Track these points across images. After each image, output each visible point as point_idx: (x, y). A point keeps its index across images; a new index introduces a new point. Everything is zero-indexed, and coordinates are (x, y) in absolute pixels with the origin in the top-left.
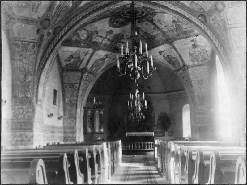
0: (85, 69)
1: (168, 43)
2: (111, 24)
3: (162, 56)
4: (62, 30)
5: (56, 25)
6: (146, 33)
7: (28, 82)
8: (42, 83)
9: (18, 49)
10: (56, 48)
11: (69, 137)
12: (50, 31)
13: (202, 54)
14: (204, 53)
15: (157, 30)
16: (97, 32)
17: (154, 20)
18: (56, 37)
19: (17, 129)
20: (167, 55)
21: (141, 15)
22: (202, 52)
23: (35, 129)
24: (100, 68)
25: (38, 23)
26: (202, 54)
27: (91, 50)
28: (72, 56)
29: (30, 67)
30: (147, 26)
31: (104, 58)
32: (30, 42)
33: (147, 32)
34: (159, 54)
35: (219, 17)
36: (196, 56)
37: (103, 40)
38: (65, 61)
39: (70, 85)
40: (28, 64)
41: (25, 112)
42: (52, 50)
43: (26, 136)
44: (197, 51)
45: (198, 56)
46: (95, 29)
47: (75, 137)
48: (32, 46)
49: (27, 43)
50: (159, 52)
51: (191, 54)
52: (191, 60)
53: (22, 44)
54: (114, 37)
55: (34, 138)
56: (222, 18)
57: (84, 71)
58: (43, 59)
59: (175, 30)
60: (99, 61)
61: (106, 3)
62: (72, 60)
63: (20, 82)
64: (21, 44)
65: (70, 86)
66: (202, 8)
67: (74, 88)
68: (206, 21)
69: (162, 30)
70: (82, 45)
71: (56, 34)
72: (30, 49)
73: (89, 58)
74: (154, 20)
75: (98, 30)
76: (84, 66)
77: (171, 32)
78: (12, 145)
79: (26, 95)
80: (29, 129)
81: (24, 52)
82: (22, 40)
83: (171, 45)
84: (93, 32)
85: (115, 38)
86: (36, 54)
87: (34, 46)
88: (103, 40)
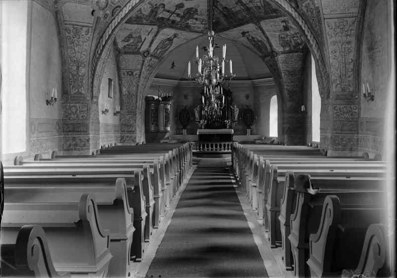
0: (148, 51)
1: (253, 23)
3: (246, 37)
5: (115, 4)
6: (225, 8)
9: (69, 35)
10: (114, 33)
12: (108, 12)
13: (295, 38)
14: (297, 37)
18: (114, 19)
20: (252, 37)
22: (295, 35)
23: (90, 132)
24: (167, 50)
26: (295, 38)
27: (155, 28)
28: (130, 36)
32: (83, 26)
35: (313, 4)
37: (170, 16)
38: (123, 41)
39: (128, 72)
40: (81, 53)
41: (78, 111)
44: (289, 34)
45: (290, 40)
48: (86, 31)
50: (242, 33)
51: (281, 37)
52: (282, 46)
53: (74, 28)
54: (185, 12)
56: (317, 6)
57: (146, 55)
58: (99, 46)
62: (132, 40)
63: (72, 75)
65: (128, 72)
67: (134, 76)
68: (298, 7)
70: (145, 21)
71: (115, 16)
73: (153, 38)
76: (147, 47)
78: (65, 150)
79: (80, 90)
82: (74, 23)
83: (256, 25)
84: (158, 5)
85: (187, 13)
87: (87, 32)
88: (170, 16)
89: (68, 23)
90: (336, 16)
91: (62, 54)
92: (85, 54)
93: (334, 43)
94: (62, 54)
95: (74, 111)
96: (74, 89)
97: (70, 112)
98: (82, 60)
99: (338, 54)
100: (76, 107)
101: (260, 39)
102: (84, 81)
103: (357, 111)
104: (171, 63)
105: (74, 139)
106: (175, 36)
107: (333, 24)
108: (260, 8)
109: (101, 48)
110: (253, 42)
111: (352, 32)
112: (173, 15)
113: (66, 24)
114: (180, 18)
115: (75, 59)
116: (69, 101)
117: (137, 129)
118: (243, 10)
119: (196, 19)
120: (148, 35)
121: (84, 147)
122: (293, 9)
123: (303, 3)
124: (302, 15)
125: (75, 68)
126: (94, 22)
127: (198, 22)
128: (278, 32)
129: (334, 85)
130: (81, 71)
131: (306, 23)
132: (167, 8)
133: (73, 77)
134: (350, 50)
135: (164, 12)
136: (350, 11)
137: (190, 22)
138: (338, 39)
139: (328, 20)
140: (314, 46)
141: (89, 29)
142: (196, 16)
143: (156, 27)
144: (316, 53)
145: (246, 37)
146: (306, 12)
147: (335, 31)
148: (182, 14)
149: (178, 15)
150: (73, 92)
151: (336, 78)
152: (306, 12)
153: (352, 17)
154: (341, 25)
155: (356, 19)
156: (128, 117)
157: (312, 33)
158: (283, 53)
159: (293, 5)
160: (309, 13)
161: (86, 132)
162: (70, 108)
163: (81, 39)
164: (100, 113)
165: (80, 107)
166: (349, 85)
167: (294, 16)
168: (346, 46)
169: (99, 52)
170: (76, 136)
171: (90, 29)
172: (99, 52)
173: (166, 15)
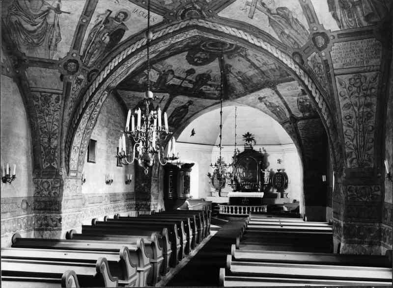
1: (270, 87)
2: (190, 60)
4: (99, 74)
5: (89, 68)
7: (53, 147)
8: (76, 148)
9: (37, 104)
11: (142, 205)
12: (81, 77)
15: (254, 69)
16: (172, 72)
17: (249, 55)
18: (92, 84)
19: (41, 209)
21: (229, 48)
24: (183, 118)
25: (60, 66)
27: (167, 95)
29: (56, 127)
30: (241, 62)
31: (187, 105)
32: (53, 93)
33: (241, 70)
34: (259, 101)
35: (319, 57)
36: (307, 105)
37: (182, 82)
41: (50, 188)
42: (87, 103)
43: (52, 219)
46: (169, 68)
47: (150, 205)
48: (56, 99)
49: (49, 94)
51: (300, 102)
53: (42, 96)
55: (63, 222)
59: (277, 69)
60: (181, 109)
61: (159, 36)
64: (40, 96)
66: (295, 42)
68: (303, 62)
69: (261, 68)
72: (53, 103)
73: (166, 105)
74: (249, 55)
75: (173, 69)
77: (273, 72)
79: (52, 164)
80: (56, 210)
81: (45, 107)
82: (40, 90)
84: (166, 71)
86: (62, 109)
87: (58, 100)
88: (182, 82)
89: (34, 89)
90: (351, 70)
91: (32, 124)
92: (57, 124)
93: (348, 106)
94: (32, 124)
95: (46, 187)
96: (46, 162)
97: (42, 188)
98: (53, 132)
99: (353, 120)
100: (48, 182)
101: (277, 104)
102: (56, 154)
103: (379, 193)
104: (191, 131)
105: (45, 218)
106: (190, 103)
107: (347, 82)
108: (275, 71)
109: (81, 111)
110: (271, 108)
111: (373, 90)
112: (185, 81)
113: (32, 91)
114: (192, 85)
115: (46, 130)
116: (41, 176)
117: (152, 196)
118: (257, 73)
119: (211, 85)
120: (160, 102)
121: (55, 227)
122: (297, 66)
123: (309, 56)
124: (308, 73)
125: (46, 140)
126: (63, 88)
127: (212, 89)
128: (295, 96)
129: (349, 160)
130: (53, 142)
131: (313, 82)
132: (176, 74)
133: (44, 150)
134: (369, 115)
135: (174, 79)
136: (370, 64)
137: (203, 88)
138: (354, 100)
139: (338, 76)
140: (323, 111)
141: (58, 97)
142: (209, 82)
143: (168, 94)
144: (326, 119)
145: (263, 103)
146: (312, 68)
147: (350, 91)
148: (194, 80)
149: (190, 82)
150: (45, 166)
151: (350, 151)
152: (312, 68)
153: (373, 71)
154: (357, 83)
155: (378, 73)
156: (143, 185)
157: (320, 94)
158: (302, 119)
159: (297, 60)
160: (316, 68)
161: (58, 210)
162: (42, 183)
163: (52, 108)
164: (133, 181)
165: (52, 183)
166: (370, 160)
167: (297, 73)
168: (365, 110)
169: (76, 122)
170: (47, 215)
171: (60, 96)
172: (76, 122)
173: (177, 82)
